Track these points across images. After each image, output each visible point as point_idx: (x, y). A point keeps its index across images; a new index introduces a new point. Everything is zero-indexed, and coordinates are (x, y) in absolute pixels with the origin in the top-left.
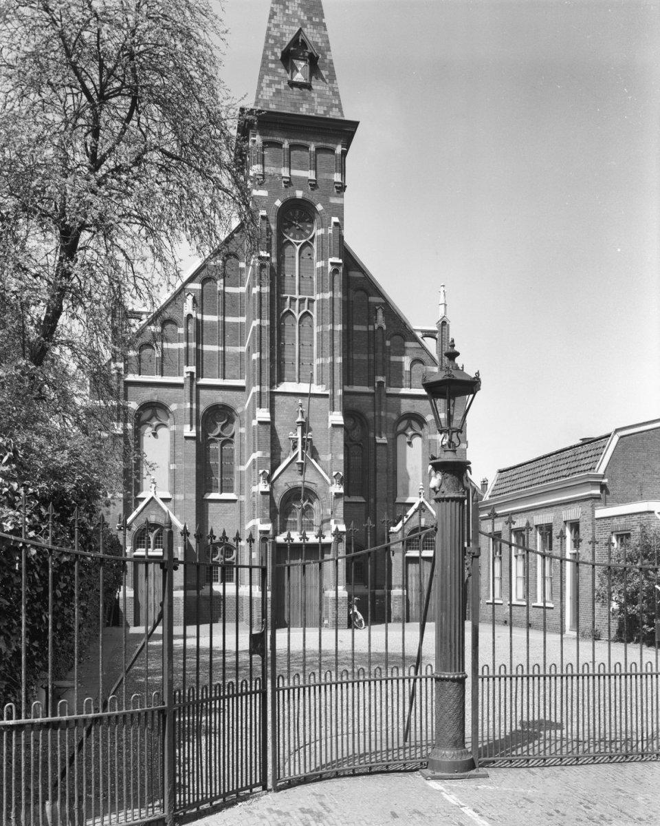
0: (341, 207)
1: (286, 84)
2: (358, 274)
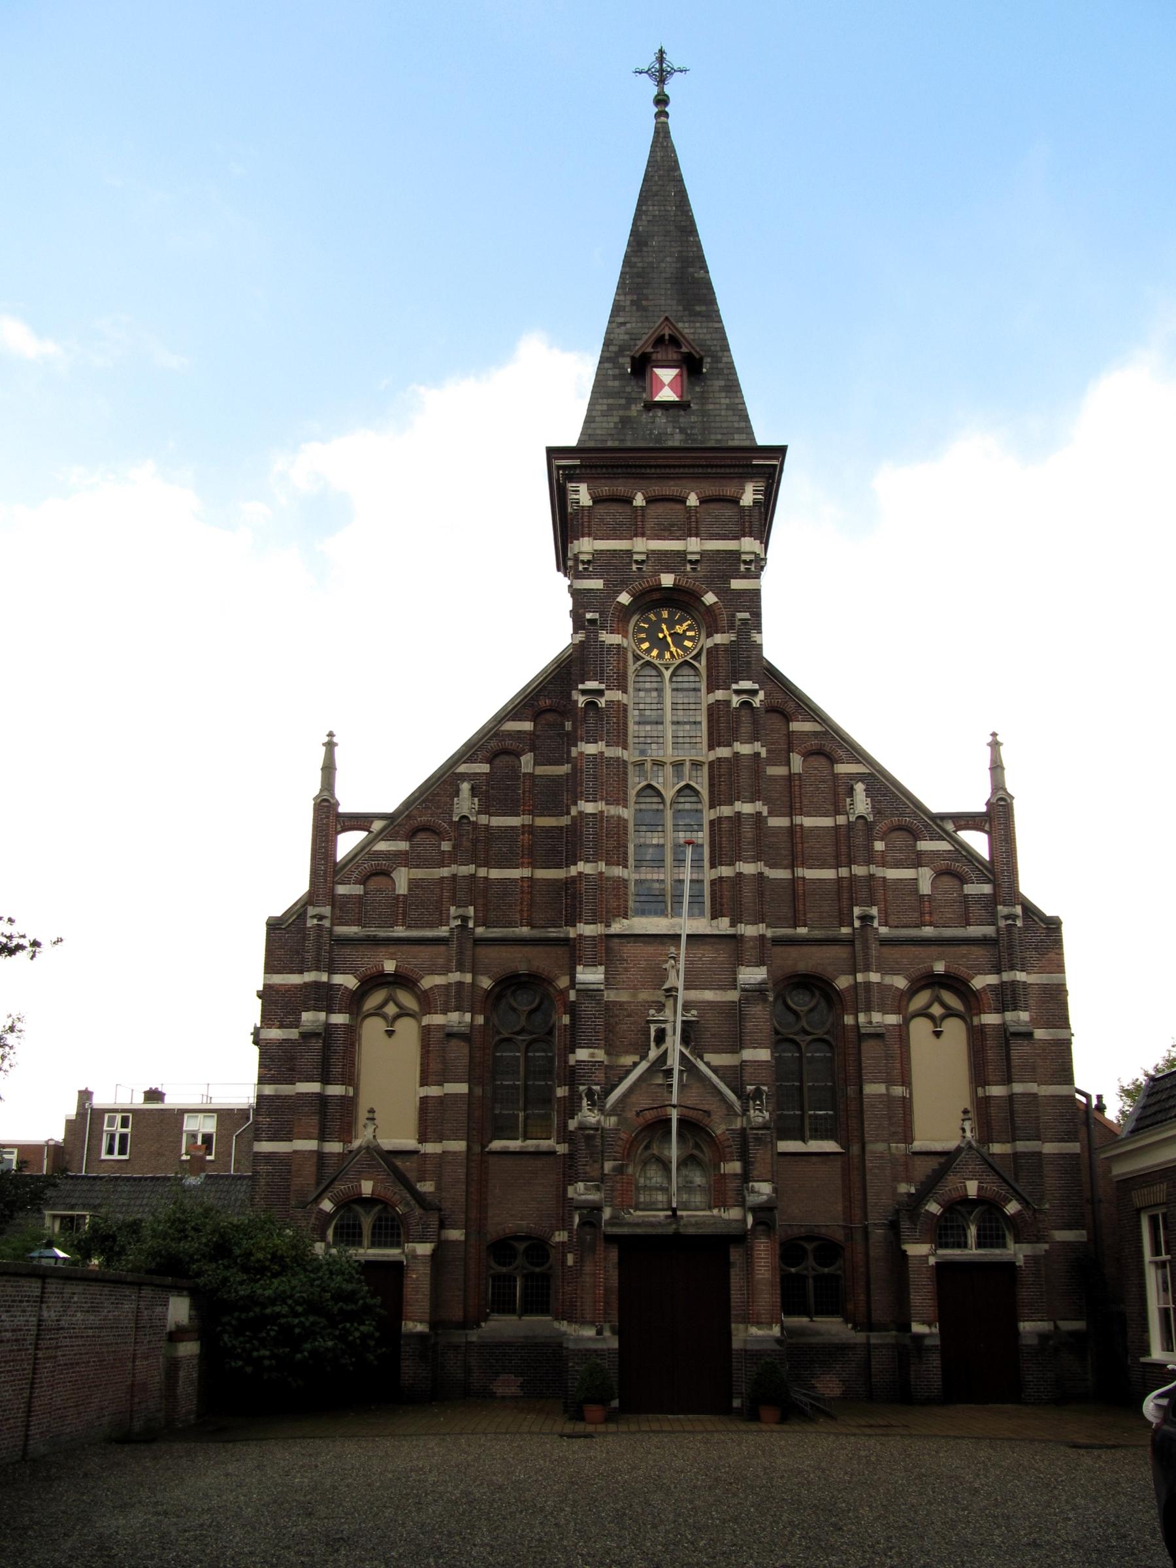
0: (755, 595)
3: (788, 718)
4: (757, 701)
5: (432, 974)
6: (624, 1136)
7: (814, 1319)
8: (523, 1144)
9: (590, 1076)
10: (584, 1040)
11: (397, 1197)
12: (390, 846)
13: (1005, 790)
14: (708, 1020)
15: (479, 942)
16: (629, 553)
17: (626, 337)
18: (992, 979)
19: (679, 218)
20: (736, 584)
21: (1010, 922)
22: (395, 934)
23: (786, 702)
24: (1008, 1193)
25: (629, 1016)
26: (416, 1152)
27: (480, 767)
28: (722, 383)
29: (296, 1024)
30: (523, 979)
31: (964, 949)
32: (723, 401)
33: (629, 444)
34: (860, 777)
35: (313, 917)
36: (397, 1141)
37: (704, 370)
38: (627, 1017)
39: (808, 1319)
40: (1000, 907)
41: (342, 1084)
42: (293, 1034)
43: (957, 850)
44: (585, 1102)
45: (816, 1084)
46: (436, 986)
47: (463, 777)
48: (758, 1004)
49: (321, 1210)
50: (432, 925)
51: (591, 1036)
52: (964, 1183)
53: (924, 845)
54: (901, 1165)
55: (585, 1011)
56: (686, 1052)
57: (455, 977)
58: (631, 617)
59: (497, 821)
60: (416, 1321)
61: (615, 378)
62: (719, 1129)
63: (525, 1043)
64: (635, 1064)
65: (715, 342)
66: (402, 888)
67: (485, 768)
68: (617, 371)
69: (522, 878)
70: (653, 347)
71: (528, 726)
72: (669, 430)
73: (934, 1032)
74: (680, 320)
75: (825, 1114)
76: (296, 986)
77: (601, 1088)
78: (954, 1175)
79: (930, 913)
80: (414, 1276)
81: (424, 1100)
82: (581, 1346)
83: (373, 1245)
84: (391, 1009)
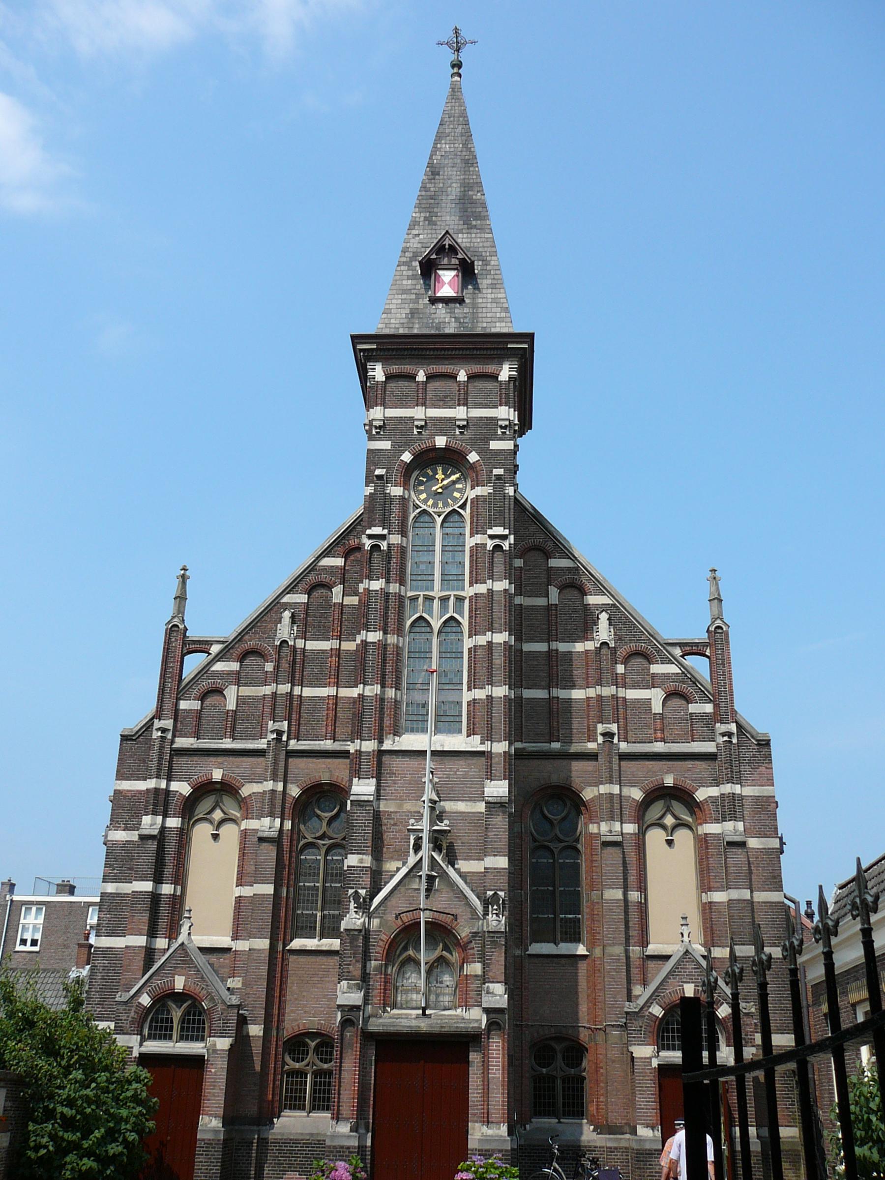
1: (426, 301)
2: (564, 563)
3: (548, 556)
4: (506, 546)
5: (251, 782)
6: (384, 937)
7: (562, 1120)
8: (319, 943)
9: (359, 881)
10: (355, 847)
11: (204, 992)
12: (224, 666)
13: (721, 619)
14: (460, 830)
15: (292, 754)
16: (412, 419)
17: (420, 245)
18: (714, 791)
19: (464, 153)
20: (494, 445)
21: (726, 738)
22: (223, 746)
23: (546, 542)
24: (720, 996)
25: (395, 825)
26: (228, 950)
27: (299, 598)
28: (489, 282)
29: (137, 827)
30: (326, 788)
31: (689, 764)
32: (489, 296)
33: (415, 331)
34: (604, 608)
35: (158, 729)
36: (215, 938)
37: (476, 272)
38: (393, 825)
39: (557, 1121)
40: (718, 725)
41: (171, 884)
42: (134, 836)
43: (683, 673)
44: (352, 905)
45: (567, 889)
46: (253, 793)
47: (286, 606)
48: (499, 815)
49: (139, 1003)
50: (254, 738)
51: (361, 843)
52: (683, 986)
53: (657, 669)
54: (636, 968)
55: (357, 820)
56: (439, 858)
57: (269, 785)
58: (413, 472)
59: (312, 645)
60: (211, 1115)
61: (408, 278)
62: (464, 932)
63: (326, 847)
64: (398, 869)
65: (486, 249)
66: (231, 705)
67: (304, 598)
68: (410, 273)
69: (329, 696)
70: (436, 255)
71: (339, 562)
72: (447, 320)
73: (666, 840)
74: (460, 231)
75: (573, 918)
76: (140, 792)
77: (367, 892)
78: (674, 979)
79: (662, 730)
80: (213, 1070)
81: (239, 900)
82: (337, 1143)
83: (182, 1038)
84: (218, 815)
